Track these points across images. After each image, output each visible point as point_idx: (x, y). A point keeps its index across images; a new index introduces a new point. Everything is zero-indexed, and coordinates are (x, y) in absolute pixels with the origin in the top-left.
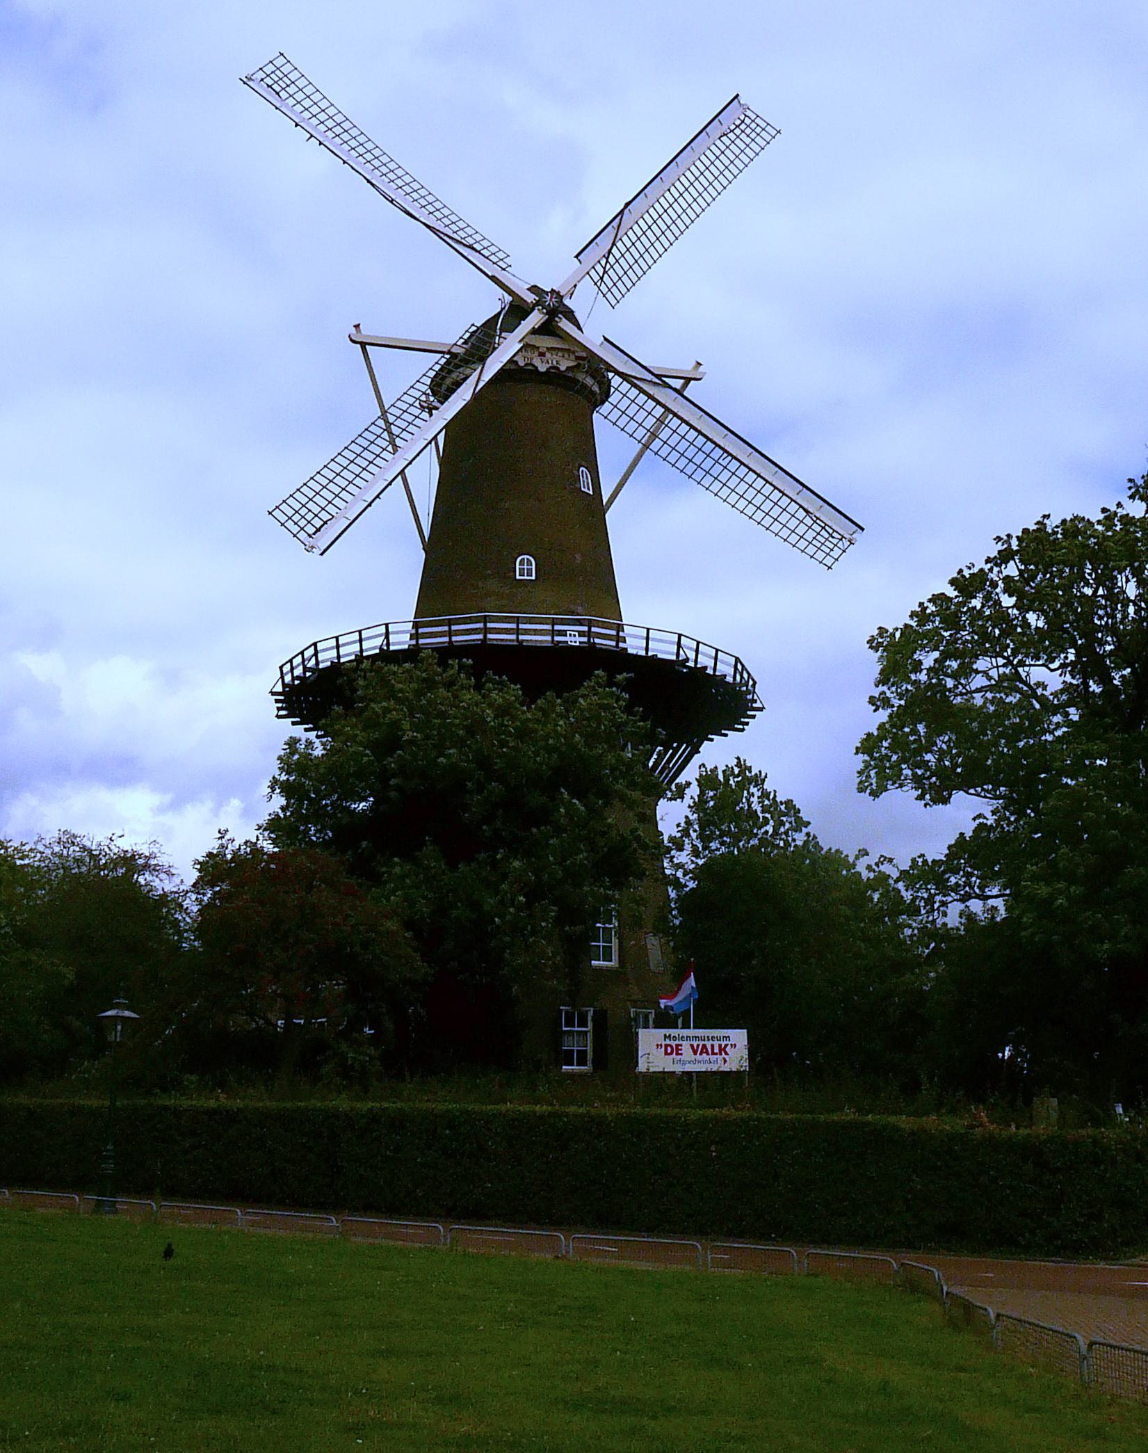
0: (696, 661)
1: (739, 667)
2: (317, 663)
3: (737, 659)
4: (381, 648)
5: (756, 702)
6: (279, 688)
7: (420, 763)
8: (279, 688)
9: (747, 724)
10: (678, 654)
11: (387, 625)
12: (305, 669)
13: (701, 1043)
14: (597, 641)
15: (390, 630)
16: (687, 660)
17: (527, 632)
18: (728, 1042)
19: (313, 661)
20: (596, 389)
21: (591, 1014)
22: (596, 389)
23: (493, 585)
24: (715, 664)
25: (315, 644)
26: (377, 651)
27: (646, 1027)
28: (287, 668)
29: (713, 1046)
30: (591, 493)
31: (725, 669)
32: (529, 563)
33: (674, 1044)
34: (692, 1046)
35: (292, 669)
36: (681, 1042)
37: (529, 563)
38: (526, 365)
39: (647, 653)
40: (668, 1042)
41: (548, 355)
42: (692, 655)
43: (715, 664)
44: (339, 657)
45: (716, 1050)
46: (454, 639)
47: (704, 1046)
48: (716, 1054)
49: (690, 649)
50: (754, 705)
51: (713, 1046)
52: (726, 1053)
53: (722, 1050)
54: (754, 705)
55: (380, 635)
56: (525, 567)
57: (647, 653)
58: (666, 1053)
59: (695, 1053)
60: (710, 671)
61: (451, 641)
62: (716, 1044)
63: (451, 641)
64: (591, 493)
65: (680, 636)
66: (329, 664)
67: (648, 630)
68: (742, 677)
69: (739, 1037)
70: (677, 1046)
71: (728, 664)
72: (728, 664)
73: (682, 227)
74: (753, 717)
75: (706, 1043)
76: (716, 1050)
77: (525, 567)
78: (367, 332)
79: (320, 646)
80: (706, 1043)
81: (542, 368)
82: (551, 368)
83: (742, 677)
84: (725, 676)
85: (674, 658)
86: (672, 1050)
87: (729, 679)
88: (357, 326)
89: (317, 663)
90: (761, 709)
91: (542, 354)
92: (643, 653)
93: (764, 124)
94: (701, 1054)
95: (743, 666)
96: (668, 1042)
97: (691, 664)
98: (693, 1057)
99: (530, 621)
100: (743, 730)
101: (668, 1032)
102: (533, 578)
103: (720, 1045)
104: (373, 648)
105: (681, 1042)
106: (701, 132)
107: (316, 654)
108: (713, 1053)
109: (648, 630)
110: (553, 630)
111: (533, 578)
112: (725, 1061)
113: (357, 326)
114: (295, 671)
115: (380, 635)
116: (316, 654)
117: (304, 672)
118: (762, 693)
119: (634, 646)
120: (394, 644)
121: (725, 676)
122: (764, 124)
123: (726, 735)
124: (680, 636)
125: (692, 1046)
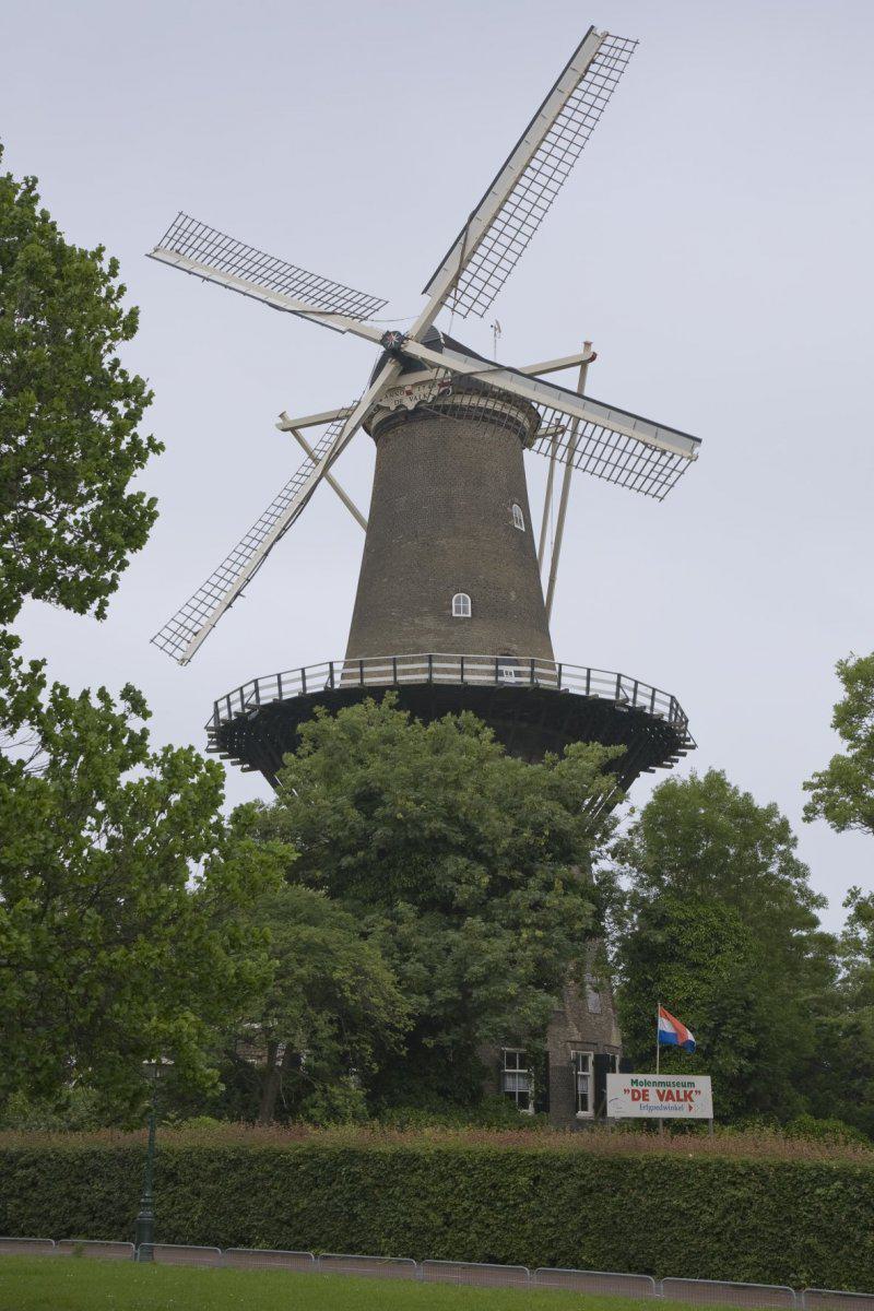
0: (634, 701)
1: (675, 706)
2: (258, 699)
3: (672, 698)
4: (326, 687)
5: (688, 740)
6: (212, 724)
7: (175, 798)
8: (212, 724)
9: (677, 761)
10: (617, 694)
11: (303, 670)
12: (244, 706)
13: (667, 1089)
14: (539, 681)
15: (283, 679)
16: (628, 700)
17: (405, 672)
18: (692, 1089)
19: (254, 698)
20: (527, 424)
21: (591, 1059)
22: (527, 424)
23: (430, 622)
24: (653, 704)
25: (256, 681)
26: (322, 689)
27: (614, 1072)
28: (222, 704)
29: (678, 1092)
30: (523, 529)
31: (662, 708)
32: (465, 601)
33: (640, 1089)
34: (658, 1091)
35: (229, 705)
36: (647, 1088)
37: (465, 601)
38: (398, 408)
39: (588, 692)
40: (635, 1087)
41: (416, 392)
42: (647, 702)
43: (653, 704)
44: (281, 694)
45: (682, 1097)
46: (435, 676)
47: (670, 1092)
48: (681, 1100)
49: (629, 689)
50: (687, 743)
51: (678, 1092)
52: (692, 1100)
53: (688, 1096)
54: (687, 743)
55: (322, 674)
56: (461, 605)
57: (588, 692)
58: (634, 1099)
59: (661, 1100)
60: (648, 711)
61: (497, 681)
62: (682, 1090)
63: (497, 681)
64: (523, 529)
65: (619, 676)
66: (271, 700)
67: (589, 670)
68: (676, 715)
69: (703, 1083)
70: (644, 1091)
71: (664, 703)
72: (664, 703)
73: (606, 474)
74: (684, 755)
75: (672, 1089)
76: (682, 1097)
77: (461, 605)
78: (294, 416)
79: (260, 683)
80: (672, 1089)
81: (411, 405)
82: (419, 403)
83: (676, 715)
84: (662, 715)
85: (613, 697)
86: (639, 1096)
87: (666, 718)
88: (281, 416)
89: (258, 699)
90: (693, 747)
91: (409, 393)
92: (583, 693)
93: (174, 229)
94: (667, 1100)
95: (678, 705)
96: (635, 1087)
97: (630, 704)
98: (659, 1103)
99: (405, 661)
100: (671, 767)
101: (634, 1076)
102: (469, 615)
103: (685, 1092)
104: (319, 686)
105: (647, 1088)
106: (503, 169)
107: (257, 690)
108: (679, 1100)
109: (589, 670)
110: (395, 670)
111: (469, 615)
112: (691, 1108)
113: (281, 416)
114: (232, 707)
115: (322, 674)
116: (257, 690)
117: (243, 708)
118: (693, 730)
119: (573, 685)
120: (311, 688)
121: (662, 715)
122: (174, 229)
123: (653, 771)
124: (619, 676)
125: (658, 1091)
